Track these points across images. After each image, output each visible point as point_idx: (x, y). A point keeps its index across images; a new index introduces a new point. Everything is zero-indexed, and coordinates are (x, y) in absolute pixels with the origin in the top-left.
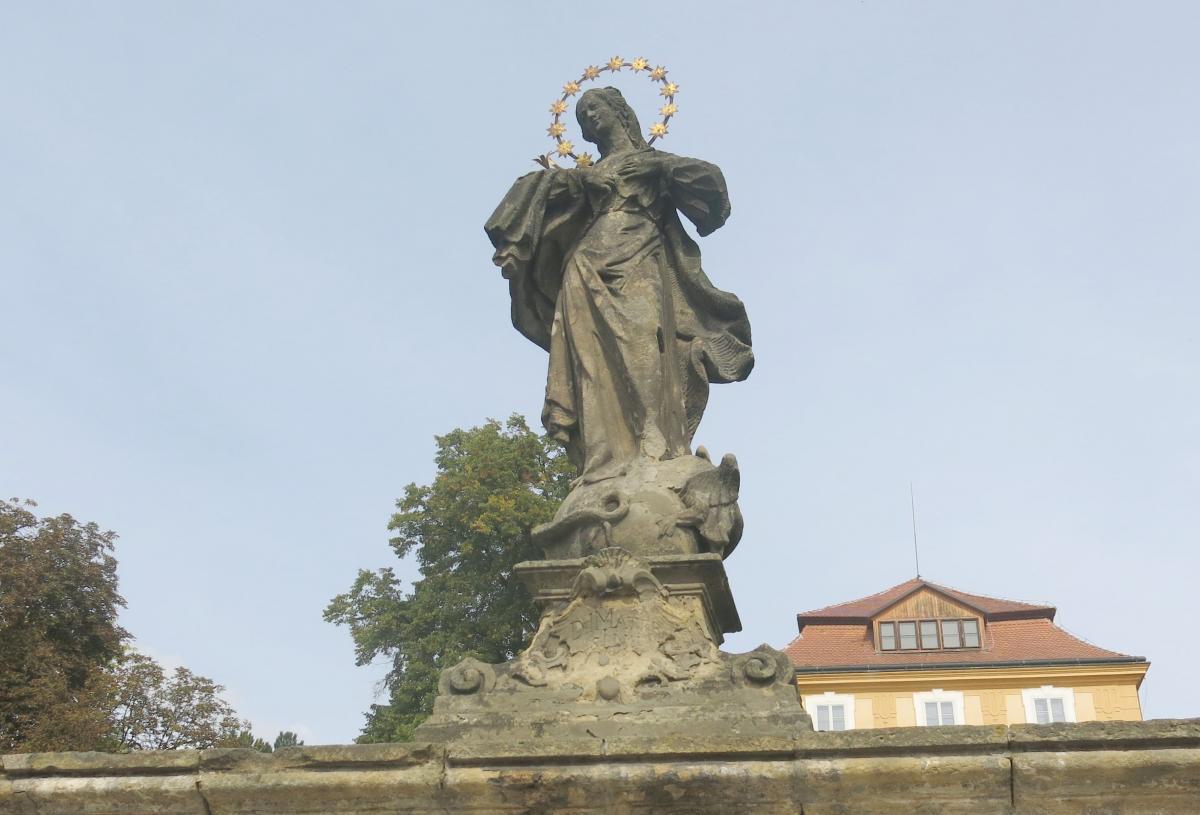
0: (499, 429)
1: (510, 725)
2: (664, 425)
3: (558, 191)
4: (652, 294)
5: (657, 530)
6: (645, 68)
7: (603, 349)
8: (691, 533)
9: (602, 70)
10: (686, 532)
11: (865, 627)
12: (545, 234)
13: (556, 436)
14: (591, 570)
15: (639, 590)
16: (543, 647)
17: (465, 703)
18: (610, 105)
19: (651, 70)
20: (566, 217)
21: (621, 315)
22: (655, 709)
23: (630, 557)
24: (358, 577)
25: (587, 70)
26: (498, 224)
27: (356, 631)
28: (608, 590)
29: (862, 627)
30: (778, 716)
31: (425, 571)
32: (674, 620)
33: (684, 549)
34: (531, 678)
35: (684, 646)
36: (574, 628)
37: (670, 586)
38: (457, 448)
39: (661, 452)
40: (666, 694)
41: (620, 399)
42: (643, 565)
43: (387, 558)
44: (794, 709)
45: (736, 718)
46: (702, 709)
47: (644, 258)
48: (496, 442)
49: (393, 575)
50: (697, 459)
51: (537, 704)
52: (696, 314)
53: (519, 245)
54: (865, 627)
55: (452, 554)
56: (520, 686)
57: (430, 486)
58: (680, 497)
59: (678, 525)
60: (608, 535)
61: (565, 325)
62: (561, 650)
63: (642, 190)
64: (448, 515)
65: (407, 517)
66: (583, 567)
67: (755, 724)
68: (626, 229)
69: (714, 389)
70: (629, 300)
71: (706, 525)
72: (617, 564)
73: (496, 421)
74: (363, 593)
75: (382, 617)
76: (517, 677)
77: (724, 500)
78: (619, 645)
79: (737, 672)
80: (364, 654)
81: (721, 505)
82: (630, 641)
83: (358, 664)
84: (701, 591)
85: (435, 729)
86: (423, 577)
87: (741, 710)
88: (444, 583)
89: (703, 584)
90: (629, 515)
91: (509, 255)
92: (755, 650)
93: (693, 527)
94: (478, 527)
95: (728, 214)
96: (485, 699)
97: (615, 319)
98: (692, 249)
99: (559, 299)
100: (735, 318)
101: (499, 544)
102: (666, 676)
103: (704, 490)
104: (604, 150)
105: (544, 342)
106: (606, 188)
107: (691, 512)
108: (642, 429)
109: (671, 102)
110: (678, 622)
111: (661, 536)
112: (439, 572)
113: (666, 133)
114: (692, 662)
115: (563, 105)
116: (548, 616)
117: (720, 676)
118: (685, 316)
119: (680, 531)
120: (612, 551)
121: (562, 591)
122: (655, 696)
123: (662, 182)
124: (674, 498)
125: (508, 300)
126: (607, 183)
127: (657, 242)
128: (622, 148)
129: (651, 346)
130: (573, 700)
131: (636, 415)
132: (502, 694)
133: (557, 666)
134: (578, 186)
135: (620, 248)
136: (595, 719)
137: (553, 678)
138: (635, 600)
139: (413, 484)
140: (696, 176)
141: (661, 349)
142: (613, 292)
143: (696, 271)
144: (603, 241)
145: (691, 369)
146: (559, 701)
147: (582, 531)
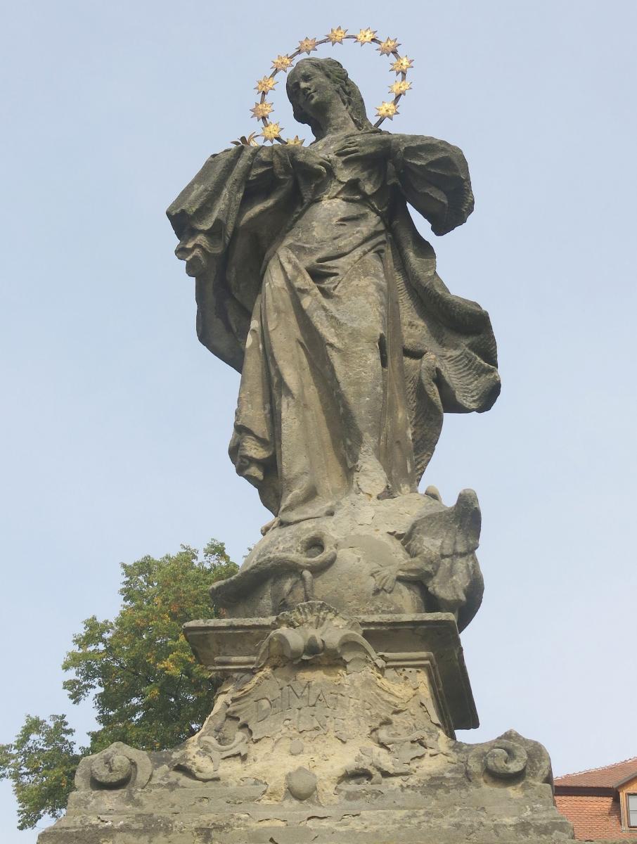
0: (195, 557)
1: (167, 830)
2: (385, 456)
3: (260, 170)
4: (376, 296)
5: (372, 583)
6: (373, 40)
7: (309, 359)
8: (417, 590)
9: (321, 42)
10: (409, 589)
11: (610, 800)
12: (242, 223)
13: (246, 473)
14: (284, 630)
15: (347, 657)
16: (218, 731)
17: (110, 800)
18: (328, 76)
19: (379, 43)
20: (270, 202)
21: (332, 317)
22: (363, 813)
23: (336, 615)
24: (25, 724)
25: (301, 43)
26: (183, 207)
27: (20, 788)
28: (305, 657)
29: (605, 799)
30: (529, 824)
31: (104, 719)
32: (391, 699)
33: (407, 607)
34: (199, 771)
35: (404, 732)
36: (259, 707)
37: (387, 655)
38: (147, 580)
39: (380, 489)
40: (378, 794)
41: (330, 423)
42: (353, 625)
43: (61, 703)
44: (551, 816)
45: (471, 826)
46: (427, 814)
47: (365, 253)
48: (191, 573)
49: (66, 724)
50: (426, 499)
51: (205, 803)
52: (429, 327)
53: (208, 233)
54: (610, 800)
55: (135, 701)
56: (184, 780)
57: (112, 620)
58: (403, 544)
59: (399, 579)
60: (308, 587)
61: (264, 336)
62: (240, 735)
63: (365, 173)
64: (132, 654)
65: (85, 655)
66: (274, 627)
67: (497, 834)
68: (343, 220)
69: (449, 418)
70: (344, 301)
71: (436, 580)
72: (319, 624)
73: (192, 548)
74: (30, 744)
75: (51, 773)
76: (181, 769)
77: (460, 549)
78: (317, 729)
79: (475, 766)
80: (28, 816)
81: (456, 554)
82: (333, 724)
83: (21, 828)
84: (428, 662)
85: (67, 833)
86: (101, 727)
87: (478, 815)
88: (124, 734)
89: (432, 654)
90: (336, 562)
91: (196, 246)
92: (499, 738)
93: (418, 582)
94: (167, 669)
95: (470, 210)
96: (136, 796)
97: (326, 324)
98: (425, 250)
99: (257, 304)
100: (477, 332)
101: (190, 692)
102: (379, 769)
103: (435, 535)
104: (319, 132)
105: (235, 359)
106: (319, 170)
107: (417, 563)
108: (355, 459)
109: (403, 79)
110: (397, 701)
111: (377, 592)
112: (121, 721)
113: (397, 113)
114: (415, 753)
115: (271, 83)
116: (226, 693)
117: (450, 771)
118: (415, 329)
119: (401, 586)
120: (312, 606)
121: (245, 659)
122: (363, 795)
123: (390, 166)
124: (396, 545)
125: (194, 307)
126: (321, 164)
127: (381, 238)
128: (341, 128)
129: (370, 356)
130: (253, 799)
131: (349, 442)
132: (159, 790)
133: (234, 756)
134: (285, 165)
135: (336, 242)
136: (282, 824)
137: (229, 771)
138: (340, 671)
139: (94, 618)
140: (431, 158)
141: (384, 363)
142: (326, 293)
143: (430, 274)
144: (314, 233)
145: (421, 392)
146: (234, 801)
147: (274, 583)
